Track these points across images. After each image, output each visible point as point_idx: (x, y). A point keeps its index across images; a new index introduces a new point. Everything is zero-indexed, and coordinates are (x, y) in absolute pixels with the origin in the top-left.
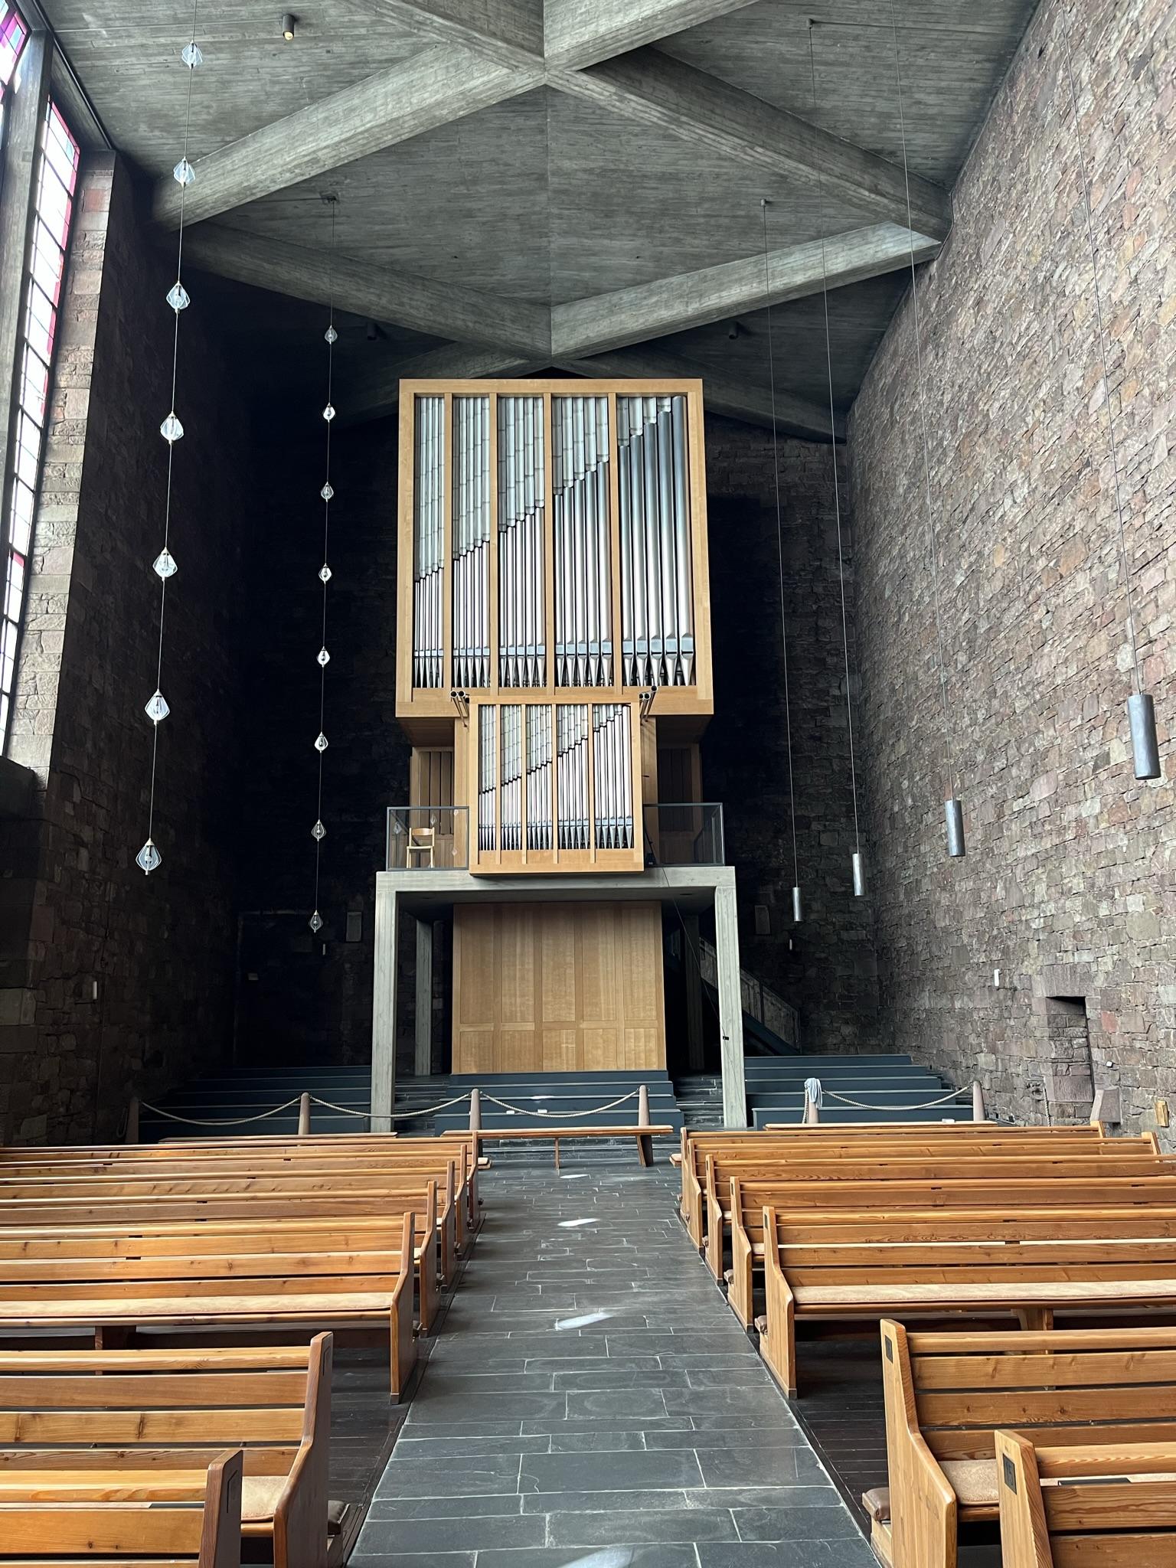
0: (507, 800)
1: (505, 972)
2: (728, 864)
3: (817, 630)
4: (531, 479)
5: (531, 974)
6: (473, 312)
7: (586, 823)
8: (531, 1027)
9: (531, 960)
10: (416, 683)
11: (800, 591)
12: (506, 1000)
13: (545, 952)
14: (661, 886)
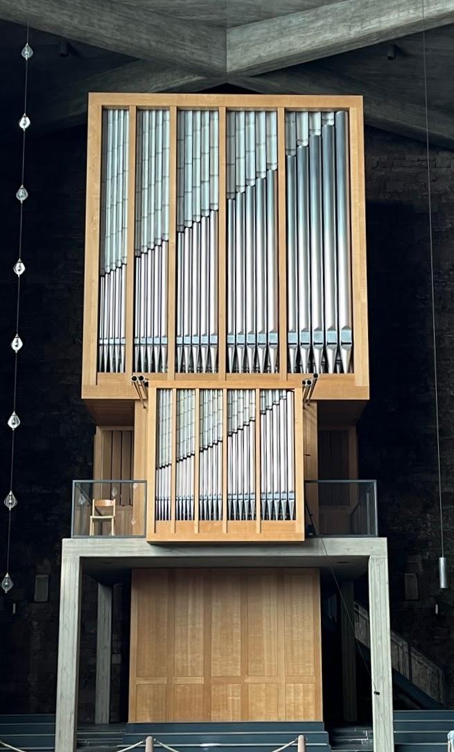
0: (181, 475)
1: (178, 630)
2: (380, 535)
5: (201, 633)
9: (201, 621)
10: (100, 368)
12: (178, 656)
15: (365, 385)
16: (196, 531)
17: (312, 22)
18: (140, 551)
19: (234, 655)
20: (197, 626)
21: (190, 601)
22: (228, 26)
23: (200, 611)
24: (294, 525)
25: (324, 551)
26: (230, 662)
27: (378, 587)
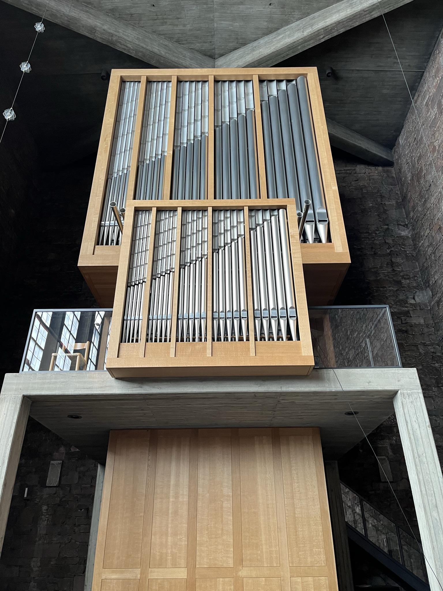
0: (158, 295)
1: (158, 505)
2: (405, 365)
3: (392, 264)
4: (199, 123)
5: (185, 507)
6: (165, 48)
7: (244, 314)
8: (182, 574)
9: (186, 492)
10: (99, 242)
11: (377, 242)
12: (156, 540)
13: (200, 482)
14: (333, 389)
15: (346, 251)
16: (172, 355)
17: (275, 38)
18: (101, 387)
19: (225, 537)
20: (180, 499)
21: (174, 464)
22: (216, 56)
23: (184, 480)
24: (298, 348)
25: (338, 385)
26: (220, 547)
27: (418, 432)
